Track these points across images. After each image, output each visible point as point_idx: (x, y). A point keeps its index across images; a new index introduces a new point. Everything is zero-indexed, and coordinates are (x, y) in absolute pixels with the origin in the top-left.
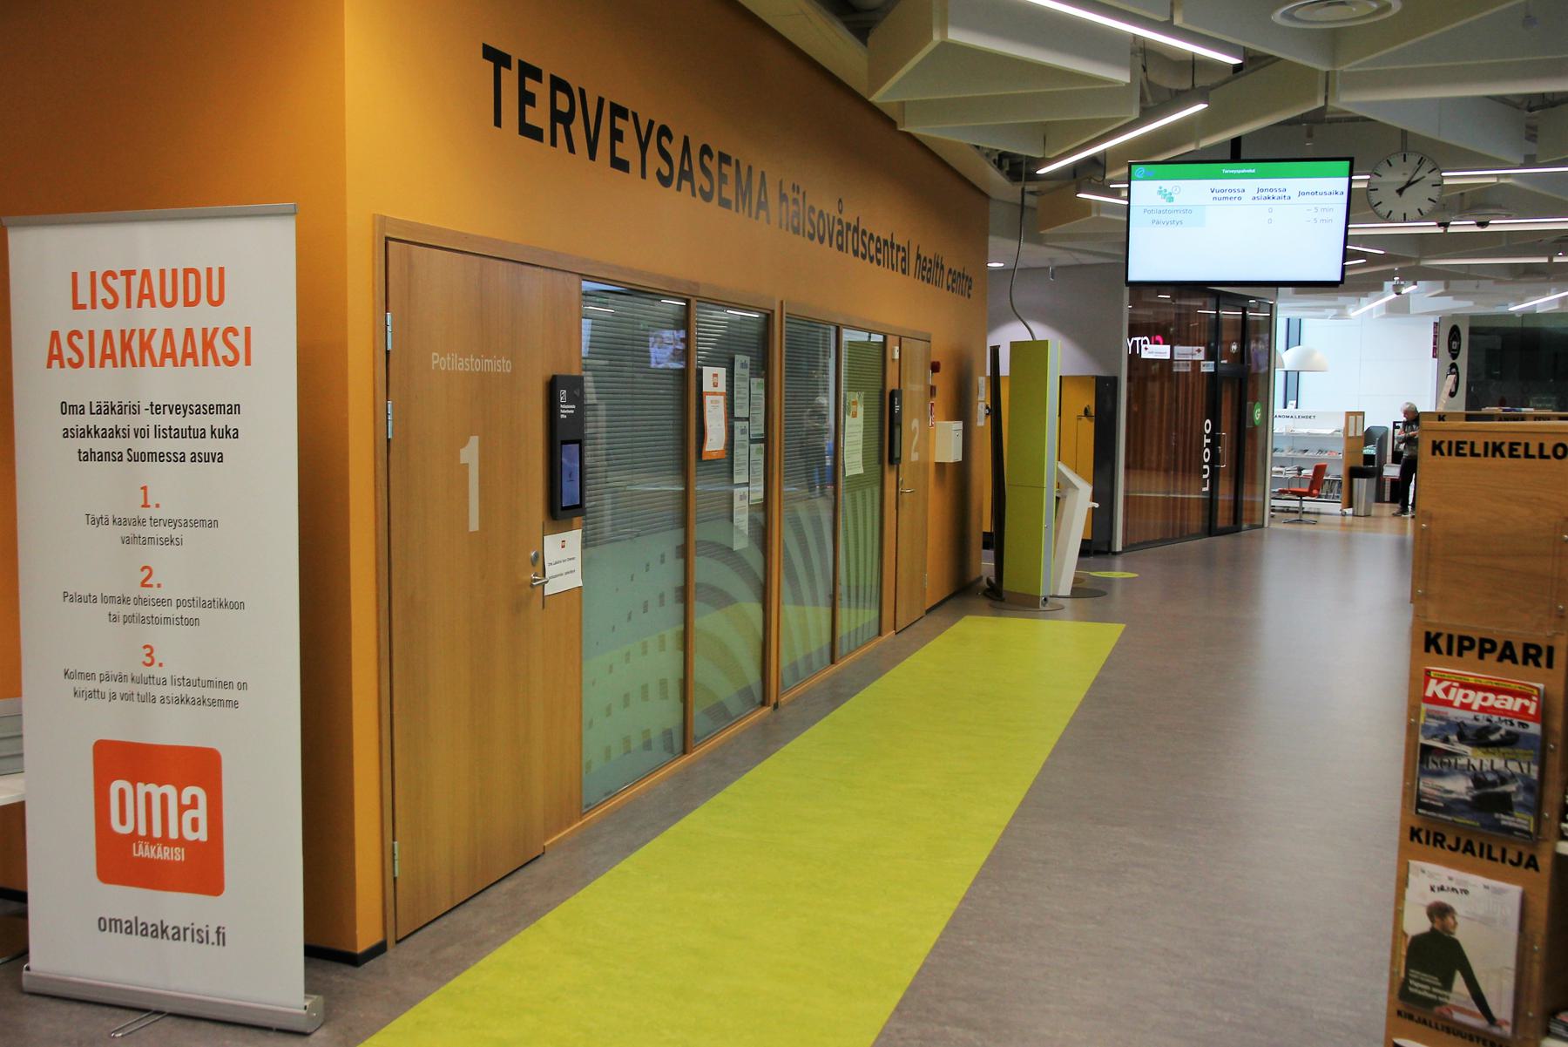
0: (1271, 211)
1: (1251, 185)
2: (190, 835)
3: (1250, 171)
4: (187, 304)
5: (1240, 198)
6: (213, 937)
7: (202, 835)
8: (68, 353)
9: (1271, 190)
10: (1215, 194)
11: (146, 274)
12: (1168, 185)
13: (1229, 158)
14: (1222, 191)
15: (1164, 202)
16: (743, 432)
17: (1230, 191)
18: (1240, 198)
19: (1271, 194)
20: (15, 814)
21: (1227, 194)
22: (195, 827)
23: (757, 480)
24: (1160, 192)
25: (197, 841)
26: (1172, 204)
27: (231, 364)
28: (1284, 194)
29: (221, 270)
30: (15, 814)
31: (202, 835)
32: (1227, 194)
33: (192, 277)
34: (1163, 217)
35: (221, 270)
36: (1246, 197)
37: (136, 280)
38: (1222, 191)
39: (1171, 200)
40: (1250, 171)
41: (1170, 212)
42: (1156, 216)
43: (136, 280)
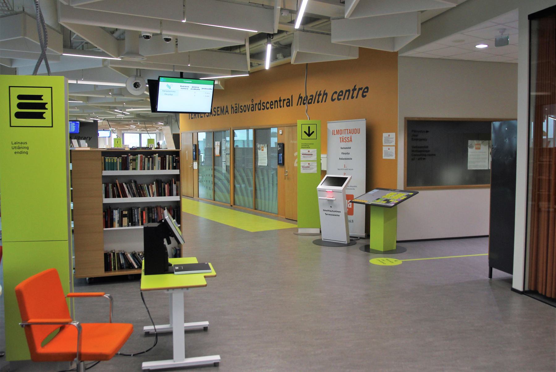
0: (195, 93)
1: (191, 85)
2: (349, 207)
3: (190, 81)
4: (355, 133)
5: (188, 89)
6: (352, 221)
7: (351, 207)
8: (344, 140)
9: (195, 87)
10: (181, 87)
11: (350, 130)
12: (169, 84)
13: (180, 77)
14: (183, 86)
15: (168, 89)
16: (224, 152)
17: (185, 87)
18: (188, 89)
19: (195, 88)
20: (1, 231)
21: (184, 87)
22: (350, 206)
23: (228, 161)
24: (167, 86)
25: (350, 208)
26: (170, 89)
27: (345, 142)
28: (198, 88)
29: (359, 129)
30: (1, 231)
31: (351, 207)
32: (184, 87)
33: (356, 130)
34: (168, 93)
35: (359, 129)
36: (189, 88)
37: (348, 130)
38: (183, 86)
39: (170, 88)
40: (190, 81)
41: (170, 91)
42: (166, 92)
43: (348, 130)
